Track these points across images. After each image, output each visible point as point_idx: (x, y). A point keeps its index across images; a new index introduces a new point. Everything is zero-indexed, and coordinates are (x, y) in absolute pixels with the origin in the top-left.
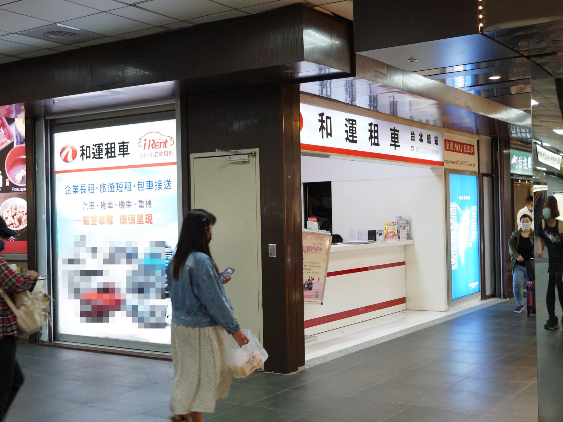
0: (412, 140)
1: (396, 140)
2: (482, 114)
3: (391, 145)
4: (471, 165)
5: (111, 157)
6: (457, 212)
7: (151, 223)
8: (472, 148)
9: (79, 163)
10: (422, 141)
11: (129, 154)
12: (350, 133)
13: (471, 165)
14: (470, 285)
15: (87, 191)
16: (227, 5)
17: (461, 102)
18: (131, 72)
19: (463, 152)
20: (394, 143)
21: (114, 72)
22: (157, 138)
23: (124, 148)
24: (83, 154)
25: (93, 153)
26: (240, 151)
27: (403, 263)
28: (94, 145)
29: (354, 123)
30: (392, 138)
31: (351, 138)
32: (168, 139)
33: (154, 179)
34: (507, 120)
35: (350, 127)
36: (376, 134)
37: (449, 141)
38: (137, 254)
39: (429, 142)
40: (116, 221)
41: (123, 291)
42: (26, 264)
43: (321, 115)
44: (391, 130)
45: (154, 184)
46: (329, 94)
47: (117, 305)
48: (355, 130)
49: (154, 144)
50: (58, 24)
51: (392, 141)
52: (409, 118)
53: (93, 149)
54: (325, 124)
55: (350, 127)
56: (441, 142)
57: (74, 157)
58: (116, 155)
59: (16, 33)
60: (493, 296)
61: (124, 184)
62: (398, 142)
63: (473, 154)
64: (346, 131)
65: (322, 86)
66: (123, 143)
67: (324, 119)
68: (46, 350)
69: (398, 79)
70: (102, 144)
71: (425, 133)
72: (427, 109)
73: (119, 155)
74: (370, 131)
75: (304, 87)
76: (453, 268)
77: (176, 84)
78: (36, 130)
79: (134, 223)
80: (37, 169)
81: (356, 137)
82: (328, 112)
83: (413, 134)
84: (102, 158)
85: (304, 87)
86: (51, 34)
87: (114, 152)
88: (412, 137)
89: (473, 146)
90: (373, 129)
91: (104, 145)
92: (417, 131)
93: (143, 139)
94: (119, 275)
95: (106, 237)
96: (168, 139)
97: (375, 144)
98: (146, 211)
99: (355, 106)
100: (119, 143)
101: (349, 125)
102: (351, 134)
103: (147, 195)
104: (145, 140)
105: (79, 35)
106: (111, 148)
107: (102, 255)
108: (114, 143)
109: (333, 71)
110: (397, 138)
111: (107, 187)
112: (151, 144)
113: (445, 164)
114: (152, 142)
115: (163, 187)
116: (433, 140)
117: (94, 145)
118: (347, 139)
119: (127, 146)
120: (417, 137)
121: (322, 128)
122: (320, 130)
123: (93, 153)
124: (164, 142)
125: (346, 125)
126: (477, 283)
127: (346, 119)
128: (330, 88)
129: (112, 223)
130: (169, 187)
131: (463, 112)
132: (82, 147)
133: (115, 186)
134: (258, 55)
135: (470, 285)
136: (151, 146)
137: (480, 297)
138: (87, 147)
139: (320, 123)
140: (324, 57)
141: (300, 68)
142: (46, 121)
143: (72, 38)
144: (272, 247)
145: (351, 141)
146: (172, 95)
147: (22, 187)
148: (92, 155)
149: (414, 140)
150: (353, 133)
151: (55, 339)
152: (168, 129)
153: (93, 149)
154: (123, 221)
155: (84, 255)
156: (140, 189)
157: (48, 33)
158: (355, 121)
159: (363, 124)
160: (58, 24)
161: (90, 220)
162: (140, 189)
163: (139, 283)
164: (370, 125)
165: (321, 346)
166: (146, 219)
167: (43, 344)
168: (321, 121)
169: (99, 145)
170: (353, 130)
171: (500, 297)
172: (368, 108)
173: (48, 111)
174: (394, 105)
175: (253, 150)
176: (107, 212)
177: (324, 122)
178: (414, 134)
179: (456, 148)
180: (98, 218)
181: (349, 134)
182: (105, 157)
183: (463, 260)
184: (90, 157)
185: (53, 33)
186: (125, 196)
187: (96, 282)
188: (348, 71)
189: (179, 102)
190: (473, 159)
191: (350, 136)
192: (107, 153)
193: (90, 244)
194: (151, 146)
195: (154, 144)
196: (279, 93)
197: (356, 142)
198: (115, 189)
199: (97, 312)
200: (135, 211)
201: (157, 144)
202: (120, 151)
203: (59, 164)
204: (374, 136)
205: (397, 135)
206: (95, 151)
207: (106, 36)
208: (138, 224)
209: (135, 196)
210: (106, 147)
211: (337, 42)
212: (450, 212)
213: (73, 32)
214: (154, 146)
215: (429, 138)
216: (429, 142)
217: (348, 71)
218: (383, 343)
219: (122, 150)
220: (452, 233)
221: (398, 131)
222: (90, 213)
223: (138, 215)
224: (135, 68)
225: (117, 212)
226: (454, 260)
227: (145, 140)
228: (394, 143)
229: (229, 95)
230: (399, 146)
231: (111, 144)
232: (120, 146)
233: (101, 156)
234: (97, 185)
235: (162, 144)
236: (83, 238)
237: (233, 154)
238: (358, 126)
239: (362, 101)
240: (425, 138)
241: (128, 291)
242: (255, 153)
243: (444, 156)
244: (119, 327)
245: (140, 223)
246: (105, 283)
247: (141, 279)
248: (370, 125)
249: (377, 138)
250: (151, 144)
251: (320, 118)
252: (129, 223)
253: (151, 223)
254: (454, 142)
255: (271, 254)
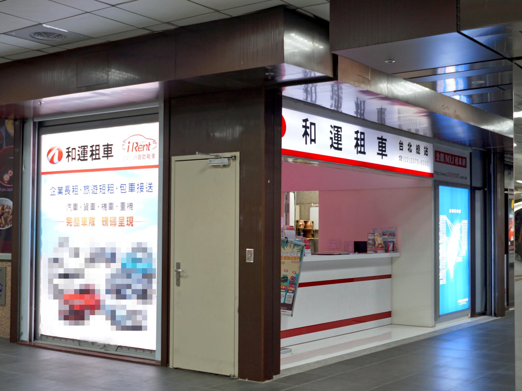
0: (400, 149)
1: (384, 149)
2: (472, 124)
3: (378, 154)
4: (462, 177)
5: (96, 159)
6: (447, 225)
7: (132, 226)
8: (464, 160)
9: (65, 164)
10: (411, 151)
11: (112, 156)
12: (335, 140)
13: (462, 177)
14: (459, 301)
15: (71, 192)
16: (206, 5)
17: (450, 110)
18: (115, 74)
19: (454, 164)
20: (381, 152)
21: (99, 75)
22: (142, 141)
23: (108, 150)
24: (69, 156)
25: (79, 155)
26: (220, 154)
27: (389, 276)
28: (79, 147)
29: (339, 130)
30: (379, 147)
31: (336, 146)
32: (151, 142)
33: (137, 182)
34: (499, 131)
35: (335, 134)
36: (362, 142)
37: (440, 153)
38: (143, 269)
39: (418, 153)
40: (98, 222)
41: (103, 292)
42: (10, 264)
43: (306, 121)
44: (378, 138)
45: (136, 187)
46: (314, 99)
47: (95, 307)
48: (341, 138)
49: (137, 147)
50: (44, 25)
51: (379, 150)
52: (397, 127)
53: (79, 151)
54: (308, 130)
55: (335, 134)
56: (431, 152)
57: (60, 158)
58: (101, 157)
59: (4, 34)
60: (483, 314)
61: (107, 186)
62: (385, 151)
63: (465, 167)
64: (331, 138)
65: (306, 91)
66: (108, 145)
67: (308, 124)
68: (25, 350)
69: (384, 87)
70: (87, 146)
71: (415, 143)
72: (420, 122)
73: (103, 157)
74: (357, 139)
75: (289, 92)
76: (441, 282)
77: (160, 86)
78: (25, 130)
79: (115, 225)
80: (23, 169)
81: (341, 144)
82: (313, 118)
83: (401, 144)
84: (86, 160)
85: (289, 92)
86: (38, 35)
87: (98, 154)
88: (400, 146)
89: (465, 158)
90: (359, 137)
91: (89, 147)
92: (406, 141)
93: (127, 142)
94: (98, 277)
95: (87, 240)
96: (151, 142)
97: (360, 152)
98: (127, 213)
99: (341, 113)
100: (103, 146)
101: (334, 132)
102: (336, 142)
103: (128, 197)
104: (129, 143)
105: (66, 37)
106: (96, 150)
107: (84, 254)
108: (99, 146)
109: (318, 74)
110: (385, 147)
111: (90, 188)
112: (134, 147)
113: (435, 175)
114: (135, 145)
115: (145, 190)
116: (422, 151)
117: (79, 147)
118: (332, 146)
119: (111, 148)
120: (406, 147)
121: (306, 134)
122: (303, 136)
123: (79, 155)
124: (147, 145)
125: (331, 132)
126: (467, 299)
127: (331, 126)
128: (316, 92)
129: (93, 225)
130: (150, 190)
131: (455, 122)
132: (68, 149)
133: (99, 187)
134: (240, 56)
135: (459, 301)
136: (134, 149)
137: (470, 314)
138: (73, 149)
139: (304, 129)
140: (308, 60)
141: (285, 71)
142: (34, 123)
143: (58, 40)
144: (250, 251)
145: (335, 148)
146: (156, 99)
147: (9, 187)
148: (77, 157)
149: (402, 149)
150: (338, 140)
151: (35, 338)
152: (151, 132)
153: (79, 151)
154: (105, 222)
155: (65, 255)
156: (122, 191)
157: (35, 34)
158: (341, 128)
159: (349, 131)
160: (44, 25)
161: (73, 221)
162: (122, 191)
163: (117, 285)
164: (357, 132)
165: (297, 355)
166: (127, 221)
167: (23, 344)
168: (305, 127)
169: (84, 147)
170: (338, 137)
171: (491, 315)
172: (355, 115)
173: (37, 114)
174: (381, 112)
175: (233, 154)
176: (90, 214)
177: (308, 127)
178: (402, 144)
179: (447, 160)
180: (81, 220)
181: (334, 141)
182: (90, 159)
183: (452, 276)
184: (75, 159)
185: (39, 34)
186: (107, 198)
187: (77, 284)
188: (330, 74)
189: (163, 105)
190: (466, 172)
191: (335, 143)
192: (92, 155)
193: (72, 244)
194: (134, 149)
195: (137, 147)
196: (262, 96)
197: (340, 149)
198: (99, 191)
199: (75, 315)
200: (117, 213)
201: (141, 147)
202: (104, 154)
203: (45, 166)
204: (360, 144)
205: (385, 144)
206: (80, 153)
207: (91, 38)
208: (119, 226)
209: (117, 198)
210: (91, 149)
211: (321, 47)
212: (439, 225)
213: (59, 33)
214: (137, 148)
215: (418, 148)
216: (418, 153)
217: (330, 74)
218: (364, 356)
219: (106, 152)
220: (440, 246)
221: (386, 140)
222: (73, 214)
223: (120, 217)
224: (127, 72)
225: (99, 214)
226: (442, 274)
227: (129, 143)
228: (381, 152)
229: (212, 98)
230: (386, 155)
231: (96, 146)
232: (104, 148)
233: (85, 158)
234: (81, 187)
235: (146, 147)
236: (67, 239)
237: (213, 157)
238: (343, 133)
239: (348, 107)
240: (414, 148)
241: (108, 292)
242: (235, 157)
243: (435, 167)
244: (96, 329)
245: (121, 225)
246: (86, 285)
247: (120, 281)
248: (357, 132)
249: (363, 146)
250: (134, 147)
251: (304, 124)
252: (111, 225)
253: (132, 226)
254: (445, 154)
255: (248, 259)
